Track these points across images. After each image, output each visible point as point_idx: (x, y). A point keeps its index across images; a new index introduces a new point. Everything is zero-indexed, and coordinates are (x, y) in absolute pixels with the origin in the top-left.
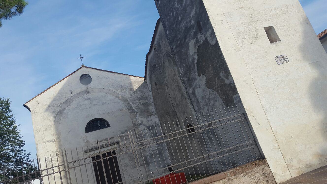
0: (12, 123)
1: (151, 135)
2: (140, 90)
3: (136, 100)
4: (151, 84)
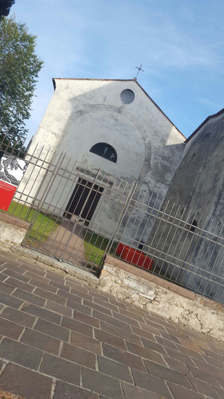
0: (31, 89)
1: (148, 201)
2: (172, 149)
3: (159, 156)
4: (189, 151)
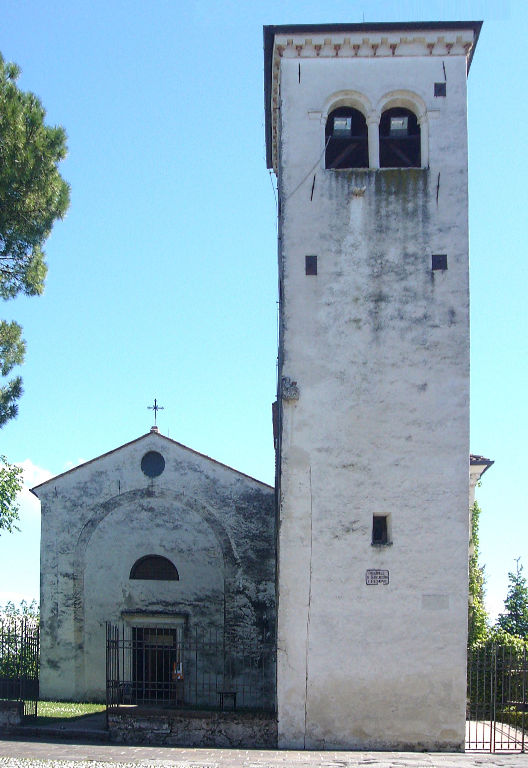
3: (245, 538)
